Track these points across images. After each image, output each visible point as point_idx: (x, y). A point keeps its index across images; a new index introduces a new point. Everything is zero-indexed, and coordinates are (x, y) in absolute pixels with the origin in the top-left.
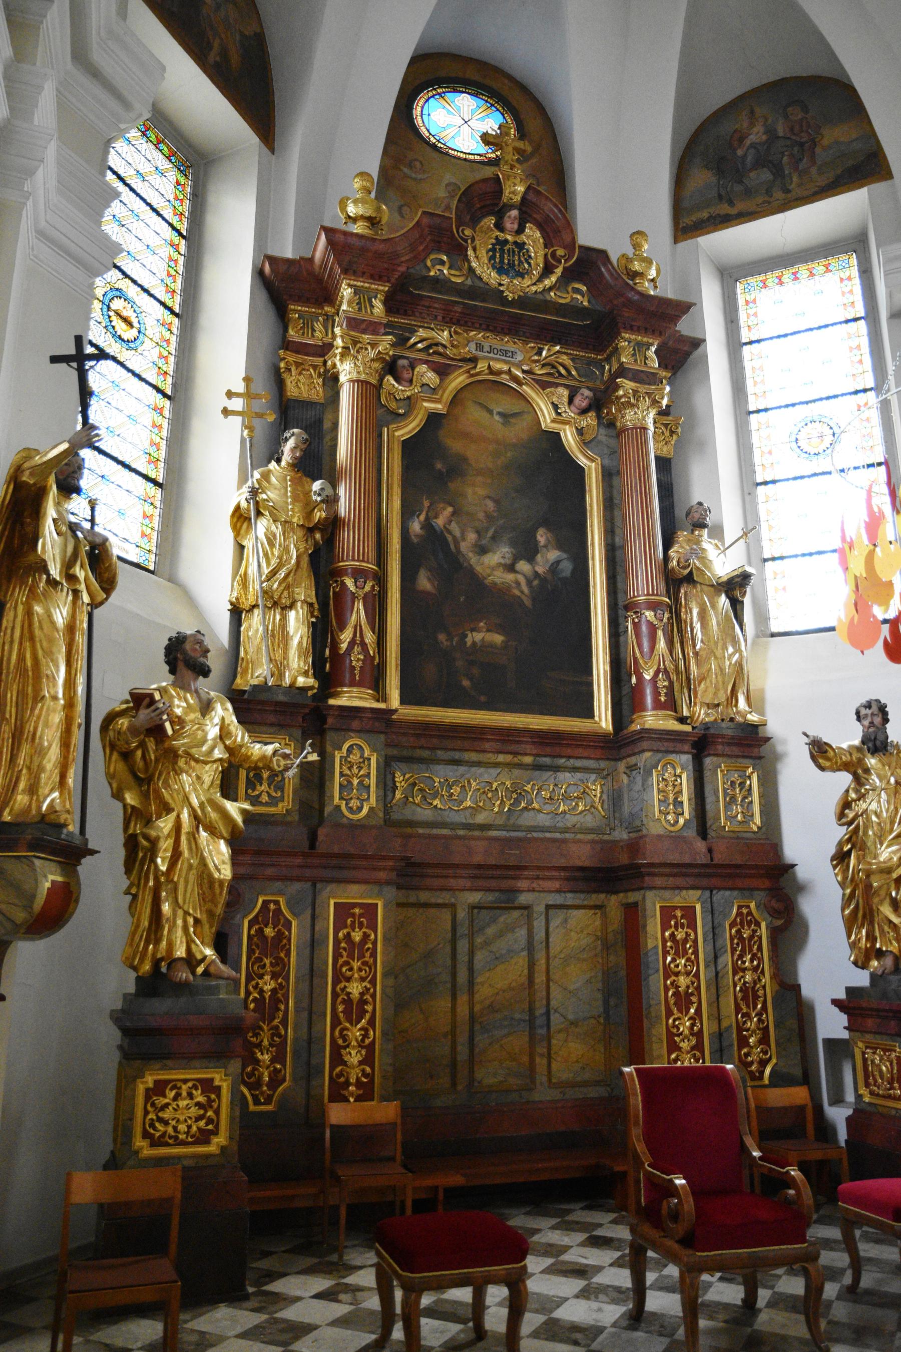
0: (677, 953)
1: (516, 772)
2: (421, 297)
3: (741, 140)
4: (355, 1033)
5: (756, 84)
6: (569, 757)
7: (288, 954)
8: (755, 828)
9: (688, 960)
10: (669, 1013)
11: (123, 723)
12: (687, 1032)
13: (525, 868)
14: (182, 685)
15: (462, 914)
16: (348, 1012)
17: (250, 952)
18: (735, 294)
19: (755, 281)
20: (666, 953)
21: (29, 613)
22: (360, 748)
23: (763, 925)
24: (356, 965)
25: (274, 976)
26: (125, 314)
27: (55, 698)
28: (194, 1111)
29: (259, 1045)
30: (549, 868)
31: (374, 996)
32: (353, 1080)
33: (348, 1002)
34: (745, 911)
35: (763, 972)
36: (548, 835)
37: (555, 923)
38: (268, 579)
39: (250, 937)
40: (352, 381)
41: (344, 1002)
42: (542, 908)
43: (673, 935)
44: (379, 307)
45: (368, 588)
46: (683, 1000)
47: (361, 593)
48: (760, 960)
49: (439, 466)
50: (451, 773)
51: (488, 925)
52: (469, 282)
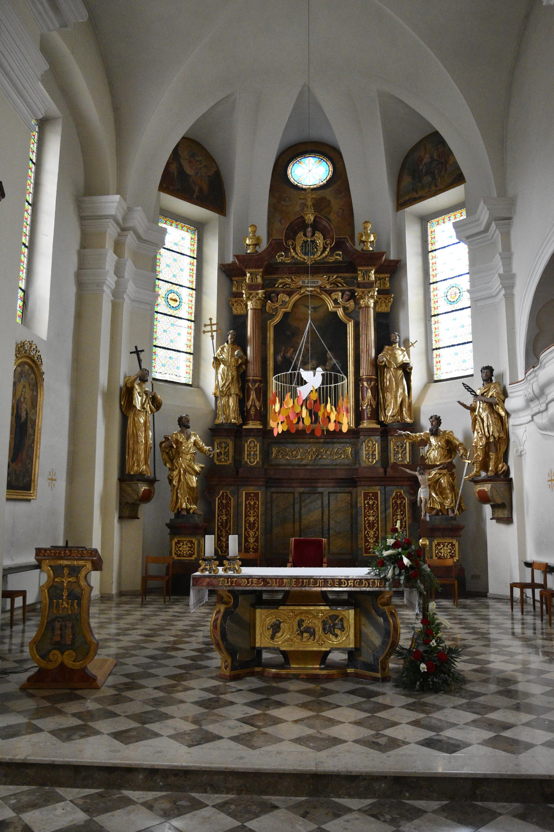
0: (369, 509)
1: (317, 445)
2: (279, 268)
3: (421, 161)
4: (251, 533)
5: (426, 135)
6: (338, 439)
7: (230, 508)
8: (406, 463)
9: (374, 511)
10: (365, 529)
11: (163, 445)
12: (372, 536)
13: (319, 479)
14: (182, 432)
15: (297, 496)
16: (249, 527)
17: (219, 508)
18: (427, 228)
19: (434, 221)
20: (365, 508)
21: (134, 419)
22: (254, 442)
23: (406, 499)
24: (252, 512)
25: (226, 515)
26: (174, 298)
27: (142, 441)
28: (187, 549)
29: (222, 536)
30: (328, 479)
31: (258, 522)
32: (251, 547)
33: (250, 523)
34: (399, 494)
35: (405, 516)
36: (329, 467)
37: (331, 499)
38: (222, 387)
39: (218, 503)
40: (251, 309)
41: (248, 523)
42: (327, 493)
43: (368, 502)
44: (259, 280)
45: (256, 386)
46: (371, 525)
47: (254, 388)
48: (404, 512)
49: (288, 333)
50: (292, 446)
51: (307, 499)
52: (293, 261)
